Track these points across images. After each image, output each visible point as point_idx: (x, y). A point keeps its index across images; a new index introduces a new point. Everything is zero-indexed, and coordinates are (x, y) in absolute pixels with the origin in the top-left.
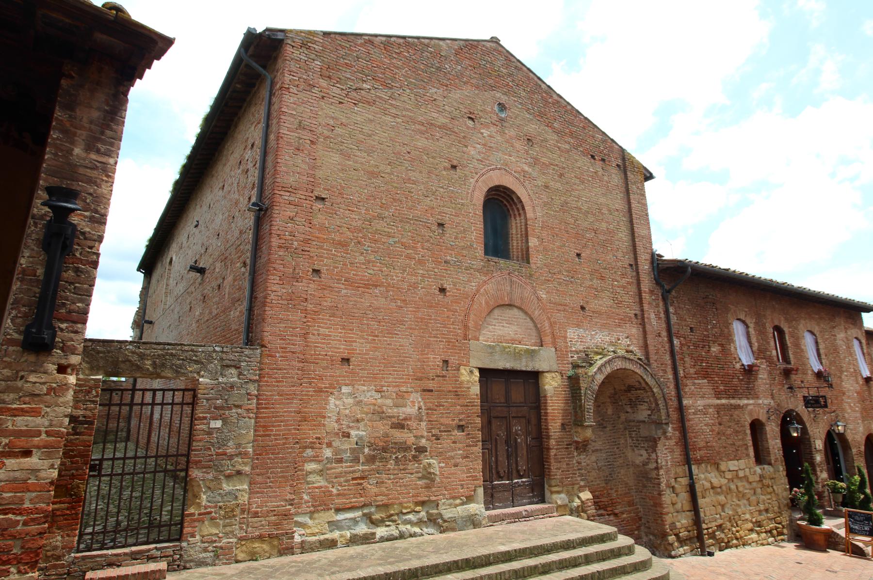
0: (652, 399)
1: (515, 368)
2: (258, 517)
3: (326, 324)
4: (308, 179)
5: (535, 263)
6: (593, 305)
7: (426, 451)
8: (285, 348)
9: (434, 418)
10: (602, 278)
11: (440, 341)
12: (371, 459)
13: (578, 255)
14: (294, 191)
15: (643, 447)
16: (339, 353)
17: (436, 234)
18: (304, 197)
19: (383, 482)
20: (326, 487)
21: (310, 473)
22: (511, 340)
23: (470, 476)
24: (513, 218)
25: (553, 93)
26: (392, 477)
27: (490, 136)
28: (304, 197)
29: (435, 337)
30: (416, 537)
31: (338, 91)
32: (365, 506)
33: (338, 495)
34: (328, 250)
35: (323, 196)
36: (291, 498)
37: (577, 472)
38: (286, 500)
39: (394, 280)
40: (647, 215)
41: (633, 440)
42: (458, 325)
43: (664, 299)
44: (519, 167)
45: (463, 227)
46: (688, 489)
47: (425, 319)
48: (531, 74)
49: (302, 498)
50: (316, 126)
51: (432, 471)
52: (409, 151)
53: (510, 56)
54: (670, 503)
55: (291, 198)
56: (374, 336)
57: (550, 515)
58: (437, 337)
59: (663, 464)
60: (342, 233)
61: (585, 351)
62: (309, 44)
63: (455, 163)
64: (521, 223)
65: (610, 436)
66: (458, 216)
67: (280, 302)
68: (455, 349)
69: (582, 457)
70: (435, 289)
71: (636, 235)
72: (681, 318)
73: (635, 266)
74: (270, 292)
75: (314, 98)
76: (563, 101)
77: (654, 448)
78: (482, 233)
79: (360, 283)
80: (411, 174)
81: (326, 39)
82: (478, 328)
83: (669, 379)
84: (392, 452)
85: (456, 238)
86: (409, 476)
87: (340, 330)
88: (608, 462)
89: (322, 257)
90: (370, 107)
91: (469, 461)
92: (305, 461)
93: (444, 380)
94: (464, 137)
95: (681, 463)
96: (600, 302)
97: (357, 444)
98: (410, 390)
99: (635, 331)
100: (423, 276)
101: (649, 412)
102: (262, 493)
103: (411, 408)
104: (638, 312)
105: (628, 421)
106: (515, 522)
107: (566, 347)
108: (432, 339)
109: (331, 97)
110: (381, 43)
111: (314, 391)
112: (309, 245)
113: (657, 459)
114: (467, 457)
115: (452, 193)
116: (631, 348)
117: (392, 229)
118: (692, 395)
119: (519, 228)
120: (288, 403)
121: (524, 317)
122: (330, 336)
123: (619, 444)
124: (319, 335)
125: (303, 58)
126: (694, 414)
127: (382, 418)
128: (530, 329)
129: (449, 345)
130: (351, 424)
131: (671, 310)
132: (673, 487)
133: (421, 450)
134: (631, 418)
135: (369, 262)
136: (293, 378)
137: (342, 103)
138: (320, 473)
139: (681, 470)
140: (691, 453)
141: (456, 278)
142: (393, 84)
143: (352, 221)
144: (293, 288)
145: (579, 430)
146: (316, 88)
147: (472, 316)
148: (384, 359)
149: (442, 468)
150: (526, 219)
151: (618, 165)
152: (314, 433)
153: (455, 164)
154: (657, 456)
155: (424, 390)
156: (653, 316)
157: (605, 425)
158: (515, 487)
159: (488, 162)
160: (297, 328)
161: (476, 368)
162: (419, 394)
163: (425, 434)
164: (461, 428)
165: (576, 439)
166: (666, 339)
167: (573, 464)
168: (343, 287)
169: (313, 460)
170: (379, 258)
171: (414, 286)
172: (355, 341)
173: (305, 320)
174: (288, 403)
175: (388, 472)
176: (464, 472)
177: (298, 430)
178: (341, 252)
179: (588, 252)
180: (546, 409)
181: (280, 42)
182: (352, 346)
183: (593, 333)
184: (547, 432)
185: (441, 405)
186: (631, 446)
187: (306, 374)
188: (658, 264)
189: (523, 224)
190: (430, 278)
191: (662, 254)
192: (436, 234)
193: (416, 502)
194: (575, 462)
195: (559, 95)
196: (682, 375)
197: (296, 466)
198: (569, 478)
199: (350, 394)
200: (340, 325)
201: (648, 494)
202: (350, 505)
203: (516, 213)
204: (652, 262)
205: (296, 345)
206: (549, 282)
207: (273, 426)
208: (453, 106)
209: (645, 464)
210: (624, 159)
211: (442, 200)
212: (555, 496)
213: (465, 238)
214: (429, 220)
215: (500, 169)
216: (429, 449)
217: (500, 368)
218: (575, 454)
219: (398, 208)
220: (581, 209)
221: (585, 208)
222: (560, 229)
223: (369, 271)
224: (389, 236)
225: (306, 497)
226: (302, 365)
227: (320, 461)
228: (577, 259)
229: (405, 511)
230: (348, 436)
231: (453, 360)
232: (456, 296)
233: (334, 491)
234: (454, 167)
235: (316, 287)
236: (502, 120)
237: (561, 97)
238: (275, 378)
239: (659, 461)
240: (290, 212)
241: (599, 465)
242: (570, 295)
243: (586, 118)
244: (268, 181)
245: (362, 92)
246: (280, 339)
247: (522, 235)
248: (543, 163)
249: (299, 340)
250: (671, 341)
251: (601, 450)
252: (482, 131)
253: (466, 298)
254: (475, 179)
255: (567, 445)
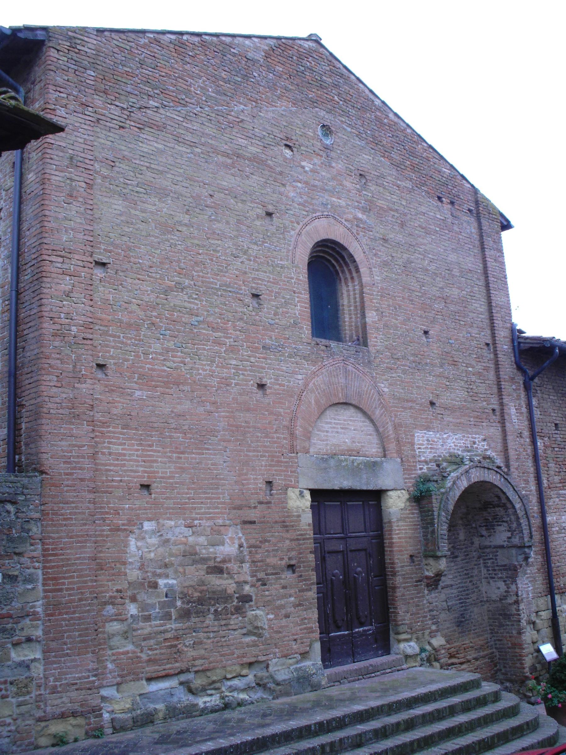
0: (513, 517)
1: (354, 488)
2: (58, 692)
3: (118, 438)
4: (86, 237)
5: (375, 346)
6: (445, 399)
7: (251, 601)
8: (71, 474)
9: (258, 557)
10: (454, 363)
11: (261, 456)
12: (185, 615)
13: (426, 333)
14: (68, 255)
15: (501, 578)
16: (137, 477)
17: (251, 308)
18: (81, 264)
19: (201, 643)
20: (134, 652)
21: (113, 635)
22: (348, 451)
23: (305, 628)
24: (343, 284)
25: (389, 111)
26: (212, 635)
27: (312, 171)
28: (81, 264)
29: (254, 451)
30: (245, 705)
31: (117, 112)
32: (182, 672)
33: (149, 661)
34: (114, 336)
35: (104, 261)
36: (95, 667)
37: (428, 614)
38: (89, 671)
39: (200, 374)
40: (505, 277)
41: (488, 570)
42: (283, 434)
43: (527, 388)
44: (351, 213)
45: (284, 298)
46: (550, 624)
47: (241, 426)
48: (361, 85)
49: (106, 667)
50: (92, 163)
51: (259, 624)
52: (212, 193)
53: (334, 61)
54: (530, 642)
55: (65, 266)
56: (179, 453)
57: (399, 668)
58: (258, 451)
59: (524, 596)
60: (131, 312)
61: (436, 461)
62: (78, 47)
63: (271, 208)
64: (354, 290)
65: (462, 568)
66: (277, 283)
67: (61, 411)
68: (281, 466)
69: (433, 595)
70: (252, 385)
71: (494, 304)
72: (544, 412)
73: (492, 345)
74: (47, 399)
75: (88, 122)
76: (402, 123)
77: (513, 578)
78: (308, 306)
79: (158, 381)
80: (216, 226)
81: (99, 39)
82: (308, 436)
83: (531, 491)
84: (210, 604)
85: (276, 314)
86: (232, 632)
87: (136, 447)
88: (460, 599)
89: (107, 346)
90: (159, 133)
91: (302, 610)
92: (106, 621)
93: (269, 508)
94: (281, 173)
95: (543, 594)
96: (453, 395)
97: (166, 596)
98: (228, 522)
99: (495, 431)
100: (236, 367)
101: (509, 534)
102: (59, 662)
103: (230, 546)
104: (496, 407)
105: (482, 548)
106: (358, 680)
107: (414, 457)
108: (251, 454)
109: (109, 120)
110: (171, 42)
111: (110, 530)
112: (90, 331)
113: (517, 592)
114: (300, 605)
115: (269, 251)
116: (488, 453)
117: (193, 303)
118: (558, 510)
119: (352, 297)
120: (81, 547)
121: (363, 419)
122: (124, 455)
123: (472, 576)
124: (110, 454)
125: (73, 66)
126: (558, 533)
127: (195, 562)
128: (370, 435)
129: (272, 461)
130: (158, 571)
131: (534, 402)
132: (534, 623)
133: (246, 599)
134: (487, 543)
135: (168, 350)
136: (84, 513)
137: (123, 128)
138: (125, 635)
139: (542, 601)
140: (555, 580)
141: (278, 369)
142: (187, 100)
143: (144, 294)
144: (76, 391)
145: (431, 561)
146: (90, 109)
147: (299, 423)
148: (194, 483)
149: (271, 620)
150: (362, 286)
151: (470, 210)
152: (114, 584)
153: (271, 211)
154: (517, 588)
155: (245, 522)
156: (513, 411)
157: (456, 554)
158: (355, 637)
159: (311, 207)
160: (84, 446)
161: (307, 489)
162: (239, 527)
163: (249, 579)
164: (291, 567)
165: (427, 573)
166: (528, 440)
167: (424, 605)
168: (136, 386)
169: (116, 620)
170: (180, 345)
171: (225, 382)
172: (156, 461)
173: (92, 435)
174: (81, 547)
175: (207, 630)
176: (297, 624)
177: (96, 581)
178: (131, 339)
179: (437, 327)
180: (392, 538)
181: (41, 43)
182: (152, 467)
183: (445, 436)
184: (394, 568)
185: (266, 541)
186: (487, 578)
187: (98, 508)
188: (519, 343)
189: (357, 292)
190: (246, 370)
191: (523, 329)
192: (251, 308)
193: (242, 664)
194: (425, 602)
195: (396, 115)
196: (546, 485)
197: (96, 627)
198: (418, 622)
199: (153, 532)
200: (136, 440)
201: (505, 634)
202: (163, 673)
203: (348, 276)
204: (513, 341)
205: (84, 469)
206: (392, 371)
207: (64, 578)
208: (264, 129)
209: (503, 598)
210: (477, 202)
211: (257, 262)
212: (402, 645)
213: (287, 313)
214: (241, 289)
215: (327, 216)
216: (254, 598)
217: (336, 488)
218: (426, 592)
219: (201, 274)
220: (427, 270)
221: (432, 267)
222: (404, 298)
223: (168, 364)
224: (191, 313)
225: (110, 666)
226: (92, 496)
227: (122, 621)
228: (424, 338)
229: (229, 676)
230: (155, 586)
231: (278, 481)
232: (279, 394)
233: (144, 657)
234: (269, 214)
235: (103, 388)
236: (326, 148)
237: (399, 117)
238: (62, 515)
239: (520, 594)
240: (66, 284)
241: (449, 604)
242: (417, 387)
243: (430, 147)
244: (29, 241)
245: (148, 111)
246: (65, 462)
247: (356, 307)
248: (381, 208)
249: (87, 464)
250: (534, 443)
251: (452, 586)
252: (303, 164)
253: (292, 396)
254: (297, 231)
255: (417, 582)
